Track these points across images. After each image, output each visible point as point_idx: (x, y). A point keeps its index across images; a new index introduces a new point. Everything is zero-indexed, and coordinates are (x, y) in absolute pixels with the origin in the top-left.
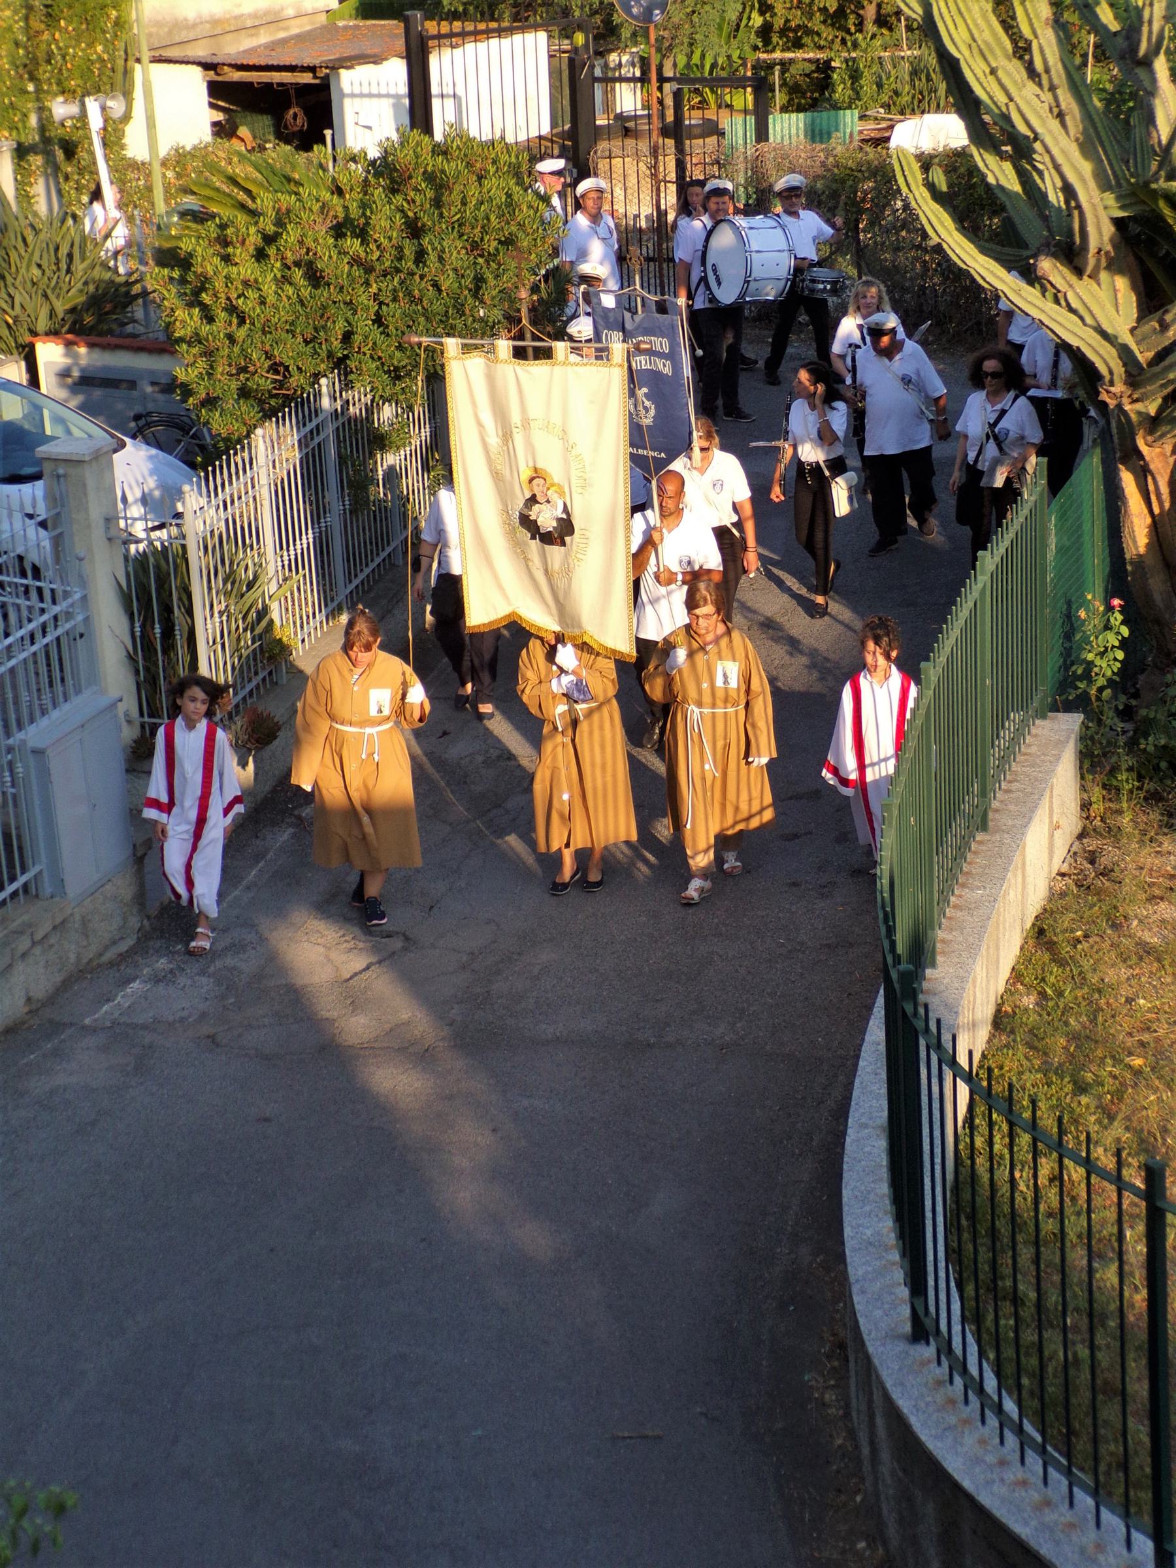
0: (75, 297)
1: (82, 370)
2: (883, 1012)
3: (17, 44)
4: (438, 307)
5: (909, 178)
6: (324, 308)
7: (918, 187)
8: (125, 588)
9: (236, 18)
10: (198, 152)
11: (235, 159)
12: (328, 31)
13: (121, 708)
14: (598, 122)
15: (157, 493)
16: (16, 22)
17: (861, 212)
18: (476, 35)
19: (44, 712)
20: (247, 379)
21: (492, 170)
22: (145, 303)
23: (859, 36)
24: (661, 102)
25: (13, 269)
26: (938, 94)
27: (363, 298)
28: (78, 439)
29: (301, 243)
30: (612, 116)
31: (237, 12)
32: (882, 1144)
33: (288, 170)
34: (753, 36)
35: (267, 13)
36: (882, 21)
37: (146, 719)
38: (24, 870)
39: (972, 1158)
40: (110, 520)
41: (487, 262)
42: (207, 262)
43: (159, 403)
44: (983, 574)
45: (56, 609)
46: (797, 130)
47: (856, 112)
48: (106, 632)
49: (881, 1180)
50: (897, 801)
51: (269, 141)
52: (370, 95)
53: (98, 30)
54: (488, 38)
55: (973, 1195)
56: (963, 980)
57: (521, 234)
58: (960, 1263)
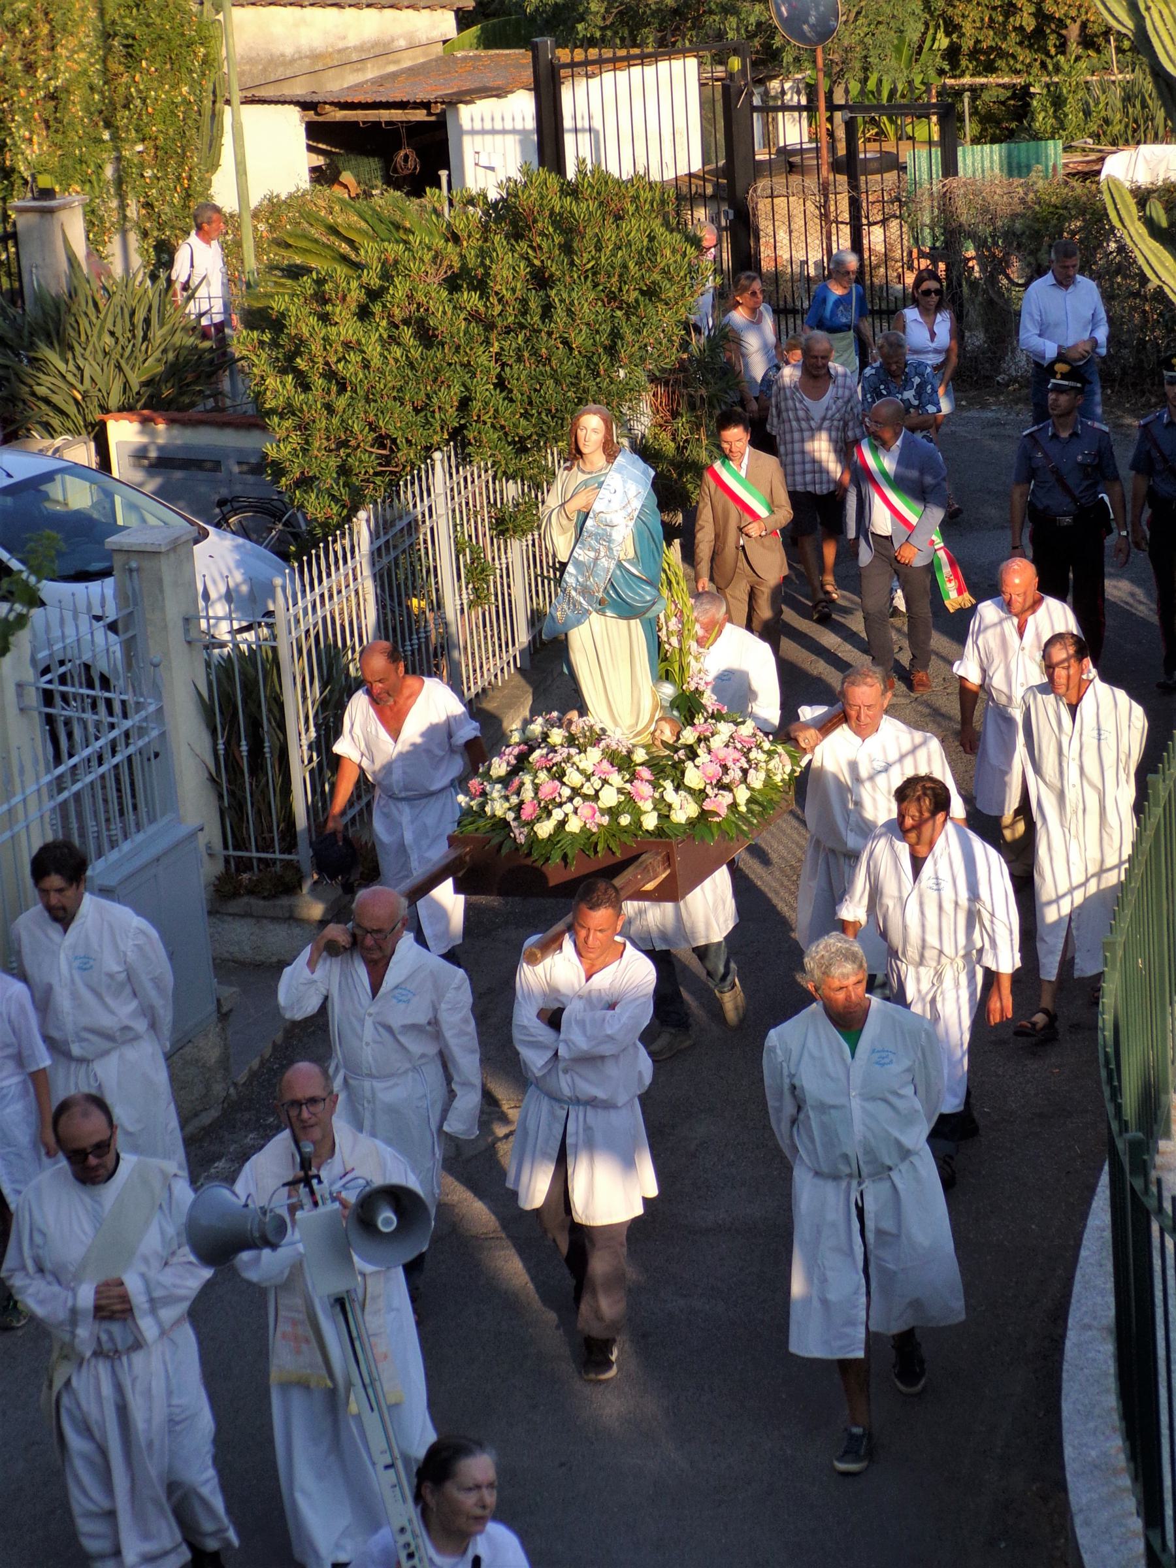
0: (152, 366)
1: (161, 448)
2: (1108, 1193)
3: (92, 88)
4: (568, 367)
5: (1123, 212)
6: (437, 371)
7: (1133, 223)
8: (206, 695)
9: (339, 51)
10: (295, 201)
11: (337, 208)
12: (446, 61)
13: (202, 839)
14: (757, 157)
15: (244, 589)
16: (92, 65)
18: (615, 63)
19: (113, 845)
20: (348, 455)
21: (631, 209)
22: (232, 373)
24: (831, 134)
25: (83, 338)
26: (1156, 122)
27: (483, 359)
28: (153, 527)
30: (773, 150)
31: (341, 45)
32: (1108, 1348)
33: (397, 218)
34: (938, 59)
35: (376, 44)
37: (231, 852)
40: (189, 620)
41: (627, 316)
42: (303, 323)
45: (128, 724)
46: (992, 162)
49: (1107, 1391)
50: (1121, 939)
51: (376, 187)
53: (184, 70)
54: (629, 66)
57: (666, 284)
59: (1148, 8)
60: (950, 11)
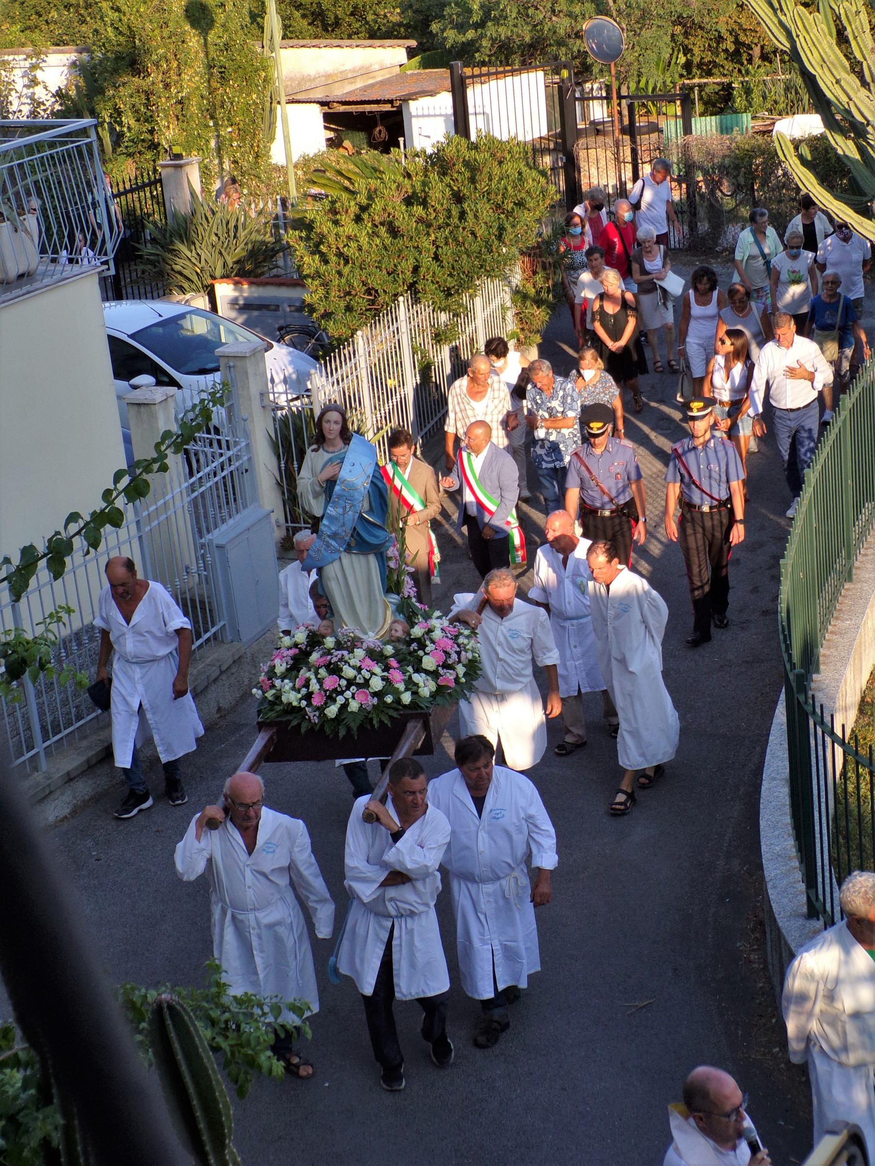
0: (240, 252)
4: (475, 247)
6: (400, 251)
12: (401, 77)
13: (273, 517)
15: (294, 376)
17: (754, 179)
19: (223, 521)
21: (508, 157)
23: (750, 67)
24: (620, 113)
27: (426, 243)
29: (384, 210)
31: (342, 69)
32: (786, 790)
34: (679, 68)
35: (362, 68)
36: (764, 57)
38: (213, 625)
39: (846, 799)
41: (507, 217)
42: (324, 226)
43: (295, 320)
44: (844, 410)
45: (230, 453)
47: (749, 115)
48: (262, 467)
52: (429, 116)
55: (847, 823)
56: (838, 681)
57: (528, 199)
58: (839, 866)
59: (798, 36)
60: (686, 42)
